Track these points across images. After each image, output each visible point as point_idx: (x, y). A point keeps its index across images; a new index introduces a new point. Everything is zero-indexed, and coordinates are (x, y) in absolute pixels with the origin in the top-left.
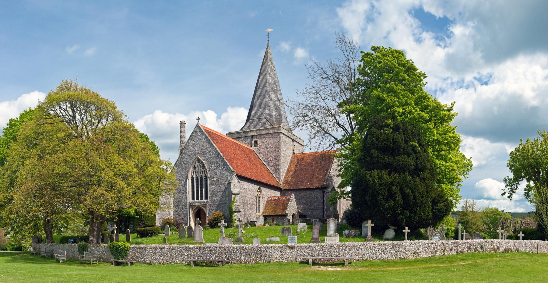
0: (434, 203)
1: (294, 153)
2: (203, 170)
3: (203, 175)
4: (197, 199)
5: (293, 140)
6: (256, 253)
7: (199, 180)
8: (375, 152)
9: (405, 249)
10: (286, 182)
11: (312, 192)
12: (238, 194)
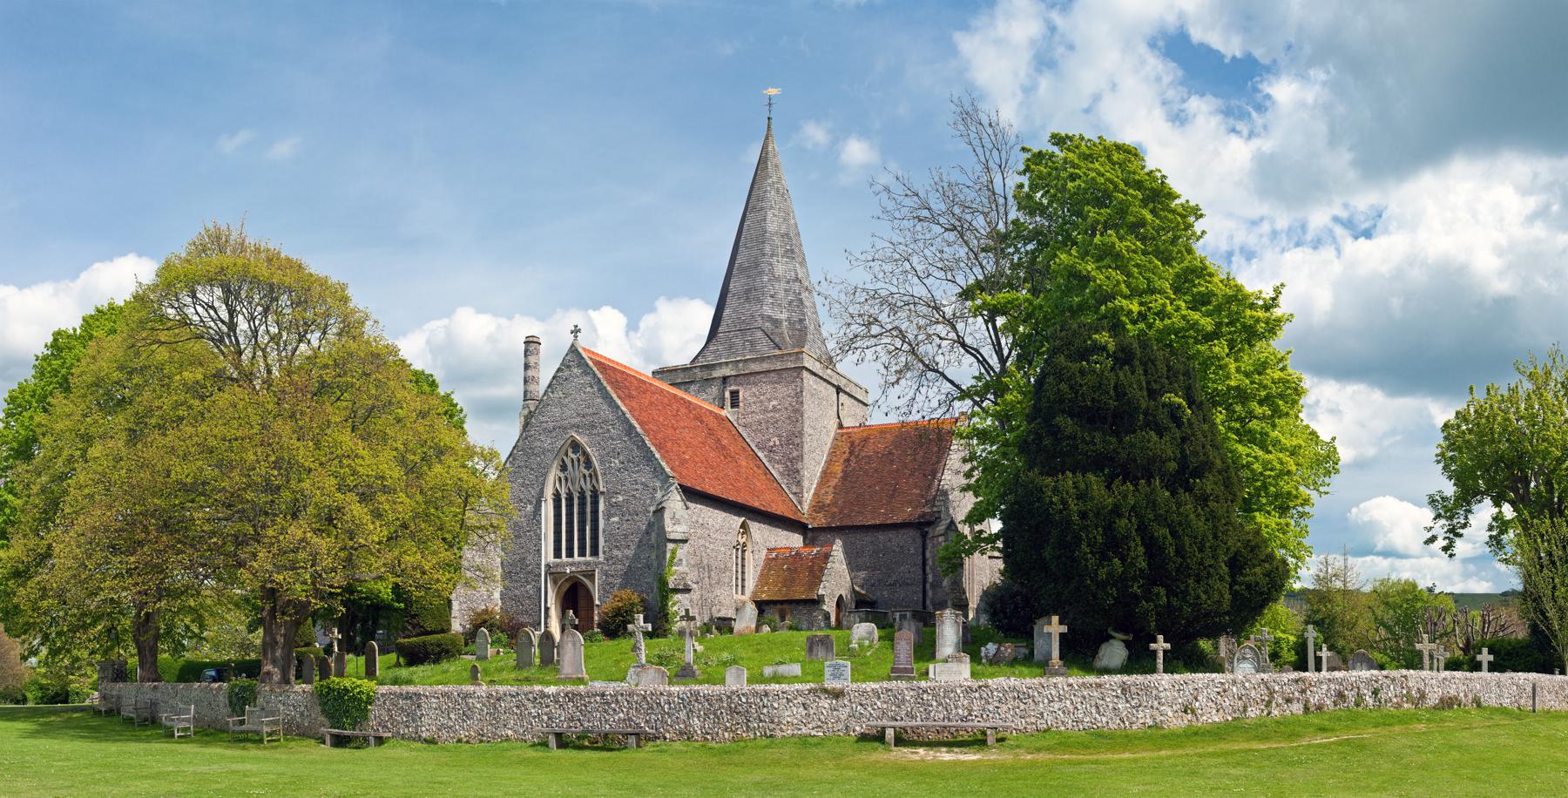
0: (1236, 565)
1: (841, 426)
3: (588, 488)
4: (570, 554)
5: (839, 390)
6: (733, 711)
7: (576, 501)
9: (1157, 698)
10: (818, 506)
11: (891, 534)
12: (685, 541)
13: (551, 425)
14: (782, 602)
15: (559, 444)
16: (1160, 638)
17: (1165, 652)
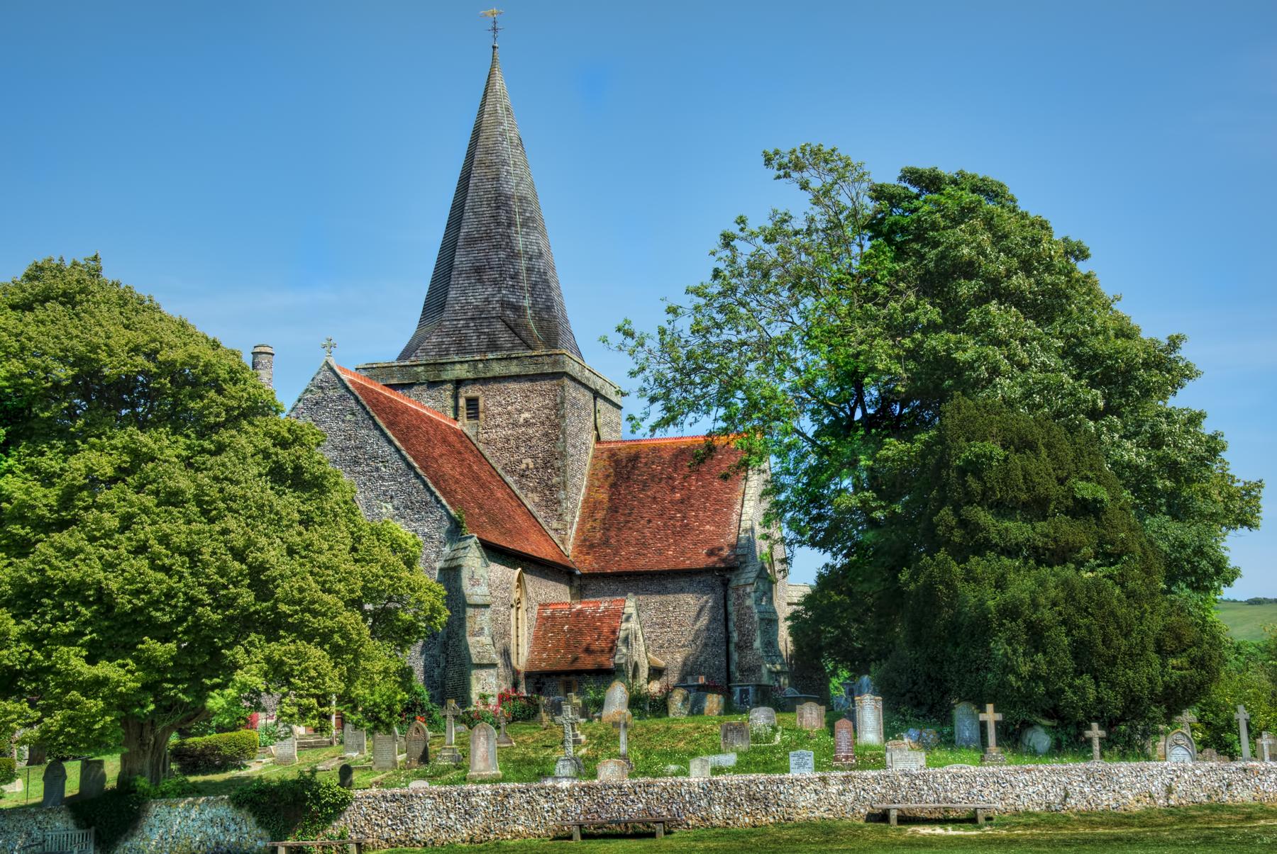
6: (752, 798)
9: (1118, 782)
10: (586, 545)
12: (487, 606)
14: (568, 673)
17: (997, 723)
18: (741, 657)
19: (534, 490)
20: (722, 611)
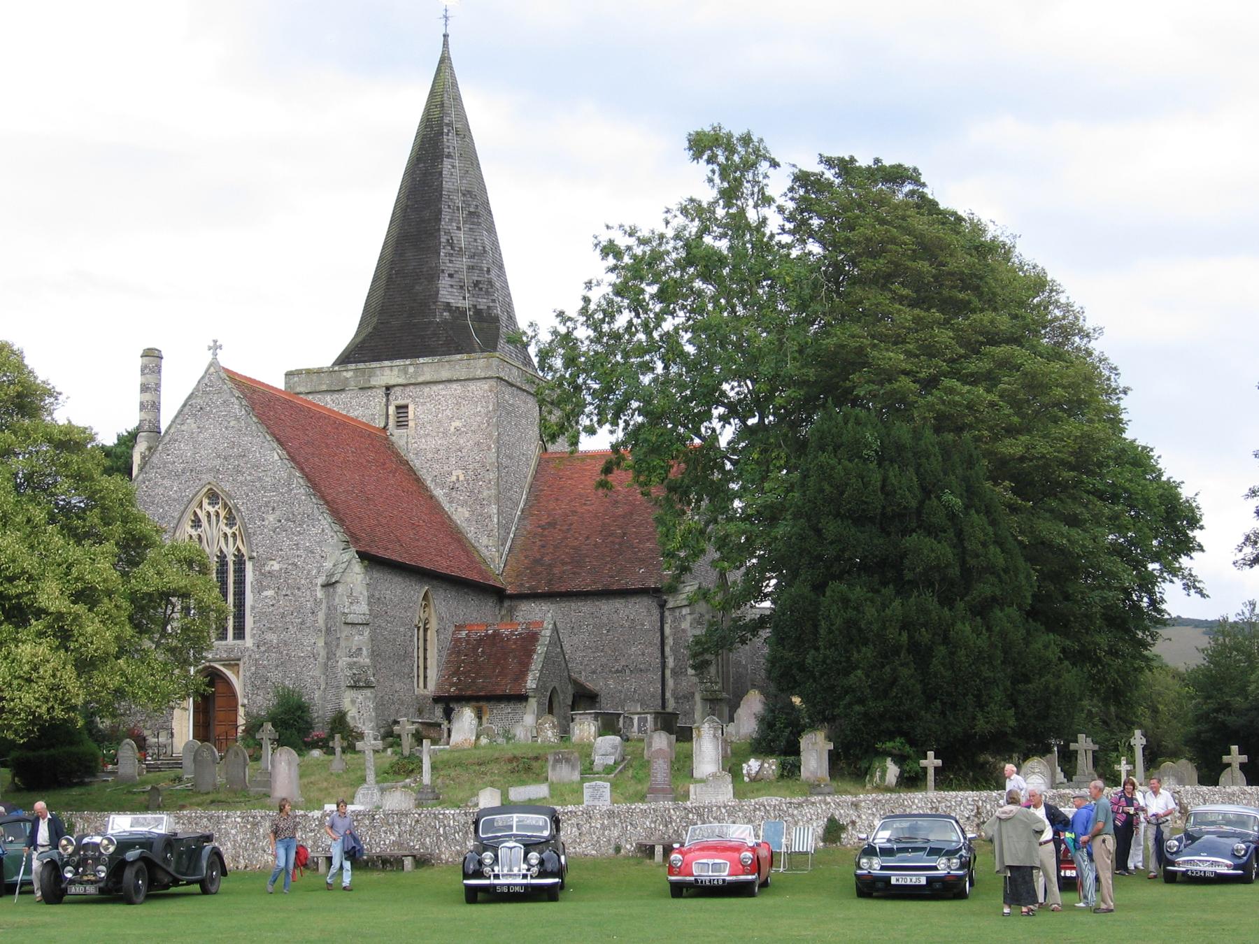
2: (229, 531)
3: (230, 551)
8: (831, 528)
11: (618, 604)
13: (180, 467)
15: (189, 493)
16: (1235, 748)
18: (676, 684)
19: (464, 504)
20: (658, 634)
